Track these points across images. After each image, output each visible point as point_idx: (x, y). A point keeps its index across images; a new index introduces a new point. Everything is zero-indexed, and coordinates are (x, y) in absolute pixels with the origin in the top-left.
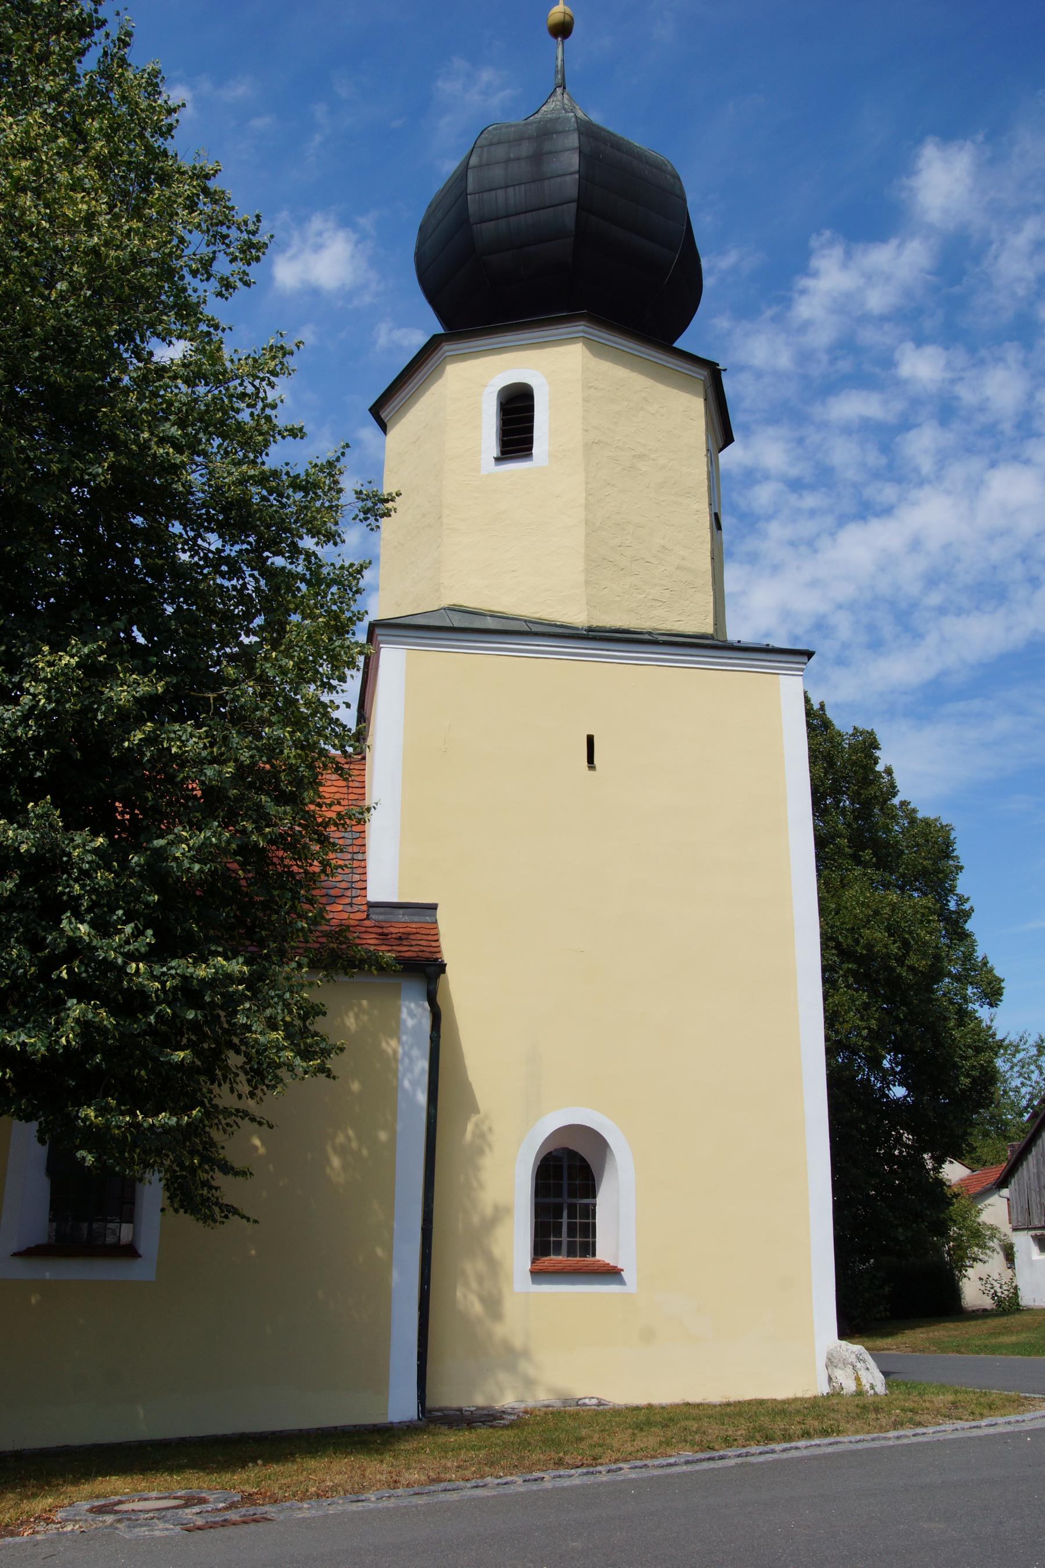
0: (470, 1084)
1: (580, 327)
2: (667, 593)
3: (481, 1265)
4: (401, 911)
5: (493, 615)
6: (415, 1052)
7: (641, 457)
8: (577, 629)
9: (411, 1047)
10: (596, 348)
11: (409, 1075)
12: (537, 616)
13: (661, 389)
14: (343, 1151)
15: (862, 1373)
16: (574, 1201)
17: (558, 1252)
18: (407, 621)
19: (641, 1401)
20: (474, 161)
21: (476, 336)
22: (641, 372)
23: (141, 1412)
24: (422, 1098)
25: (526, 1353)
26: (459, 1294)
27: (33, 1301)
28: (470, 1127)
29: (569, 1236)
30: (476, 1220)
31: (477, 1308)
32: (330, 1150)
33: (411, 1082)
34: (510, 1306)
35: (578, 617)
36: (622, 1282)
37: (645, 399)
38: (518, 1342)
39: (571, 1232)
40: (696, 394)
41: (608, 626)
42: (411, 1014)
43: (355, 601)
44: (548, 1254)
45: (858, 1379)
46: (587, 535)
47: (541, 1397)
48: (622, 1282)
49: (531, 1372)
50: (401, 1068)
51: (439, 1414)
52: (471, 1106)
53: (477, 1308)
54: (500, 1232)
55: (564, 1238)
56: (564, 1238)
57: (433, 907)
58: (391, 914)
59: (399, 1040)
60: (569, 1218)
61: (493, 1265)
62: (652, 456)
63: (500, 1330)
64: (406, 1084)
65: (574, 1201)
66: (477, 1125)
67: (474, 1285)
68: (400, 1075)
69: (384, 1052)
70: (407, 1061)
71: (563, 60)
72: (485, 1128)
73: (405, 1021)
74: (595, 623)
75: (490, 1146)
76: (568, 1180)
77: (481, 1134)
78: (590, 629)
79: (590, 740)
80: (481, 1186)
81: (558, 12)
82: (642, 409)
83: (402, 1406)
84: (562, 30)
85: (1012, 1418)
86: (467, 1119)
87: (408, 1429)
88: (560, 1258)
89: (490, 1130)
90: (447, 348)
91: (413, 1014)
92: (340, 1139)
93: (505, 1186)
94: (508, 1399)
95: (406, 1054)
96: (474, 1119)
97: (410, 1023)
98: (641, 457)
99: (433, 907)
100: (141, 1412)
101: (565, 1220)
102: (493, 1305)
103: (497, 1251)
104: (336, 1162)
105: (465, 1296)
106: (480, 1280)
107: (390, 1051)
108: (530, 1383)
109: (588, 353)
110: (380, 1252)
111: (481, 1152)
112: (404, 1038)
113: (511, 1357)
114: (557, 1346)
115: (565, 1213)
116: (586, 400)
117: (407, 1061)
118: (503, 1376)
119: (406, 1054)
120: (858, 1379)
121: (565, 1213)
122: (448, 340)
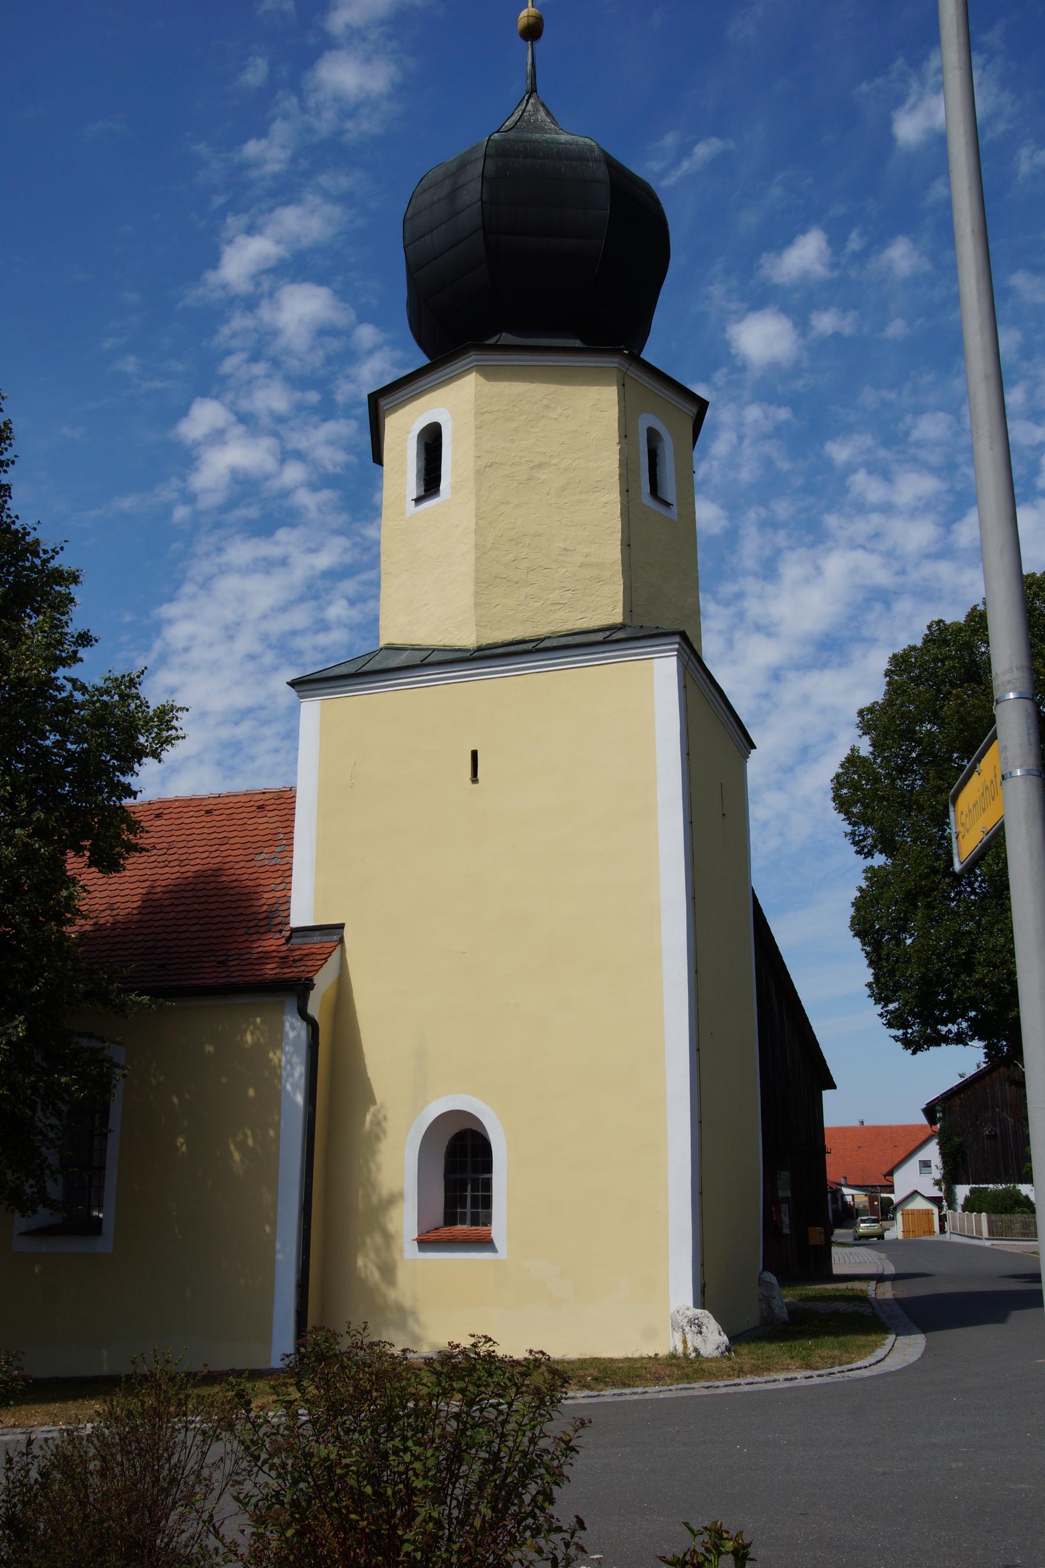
0: (369, 1079)
1: (472, 358)
2: (569, 594)
3: (378, 1238)
4: (317, 933)
5: (414, 648)
6: (295, 1059)
7: (540, 466)
8: (468, 650)
9: (292, 1056)
10: (490, 373)
11: (291, 1080)
12: (442, 643)
13: (567, 389)
14: (242, 1147)
15: (689, 1337)
16: (475, 1176)
17: (463, 1223)
18: (311, 677)
20: (408, 215)
21: (410, 382)
23: (105, 1354)
24: (300, 1099)
25: (413, 1313)
26: (360, 1262)
27: (37, 1271)
28: (369, 1117)
29: (472, 1207)
30: (374, 1199)
31: (376, 1275)
32: (232, 1148)
33: (292, 1085)
34: (402, 1275)
35: (468, 639)
37: (547, 407)
38: (408, 1303)
39: (474, 1205)
40: (613, 386)
41: (500, 641)
42: (293, 1028)
44: (455, 1224)
45: (685, 1342)
46: (477, 559)
49: (417, 1330)
50: (284, 1074)
52: (369, 1098)
53: (374, 1275)
55: (468, 1210)
56: (468, 1210)
57: (341, 926)
58: (306, 936)
59: (282, 1050)
60: (472, 1191)
61: (388, 1238)
62: (553, 462)
63: (392, 1295)
64: (289, 1087)
65: (475, 1176)
66: (374, 1115)
67: (372, 1255)
68: (283, 1081)
69: (271, 1060)
70: (288, 1067)
71: (533, 64)
72: (381, 1116)
73: (287, 1034)
74: (484, 642)
75: (384, 1132)
76: (463, 1161)
77: (377, 1123)
78: (480, 649)
79: (474, 754)
80: (379, 1168)
81: (526, 15)
82: (543, 417)
84: (533, 32)
85: (640, 1390)
86: (367, 1109)
88: (465, 1227)
89: (385, 1118)
91: (294, 1030)
92: (240, 1137)
93: (398, 1168)
95: (289, 1062)
96: (372, 1109)
97: (292, 1035)
98: (540, 466)
99: (341, 926)
100: (105, 1354)
101: (469, 1193)
102: (388, 1271)
103: (391, 1228)
104: (237, 1156)
105: (366, 1266)
106: (377, 1251)
107: (276, 1060)
109: (481, 380)
110: (268, 1229)
111: (378, 1139)
112: (287, 1048)
113: (402, 1315)
115: (469, 1187)
116: (478, 427)
117: (288, 1067)
119: (289, 1062)
120: (685, 1342)
121: (469, 1187)
122: (382, 396)
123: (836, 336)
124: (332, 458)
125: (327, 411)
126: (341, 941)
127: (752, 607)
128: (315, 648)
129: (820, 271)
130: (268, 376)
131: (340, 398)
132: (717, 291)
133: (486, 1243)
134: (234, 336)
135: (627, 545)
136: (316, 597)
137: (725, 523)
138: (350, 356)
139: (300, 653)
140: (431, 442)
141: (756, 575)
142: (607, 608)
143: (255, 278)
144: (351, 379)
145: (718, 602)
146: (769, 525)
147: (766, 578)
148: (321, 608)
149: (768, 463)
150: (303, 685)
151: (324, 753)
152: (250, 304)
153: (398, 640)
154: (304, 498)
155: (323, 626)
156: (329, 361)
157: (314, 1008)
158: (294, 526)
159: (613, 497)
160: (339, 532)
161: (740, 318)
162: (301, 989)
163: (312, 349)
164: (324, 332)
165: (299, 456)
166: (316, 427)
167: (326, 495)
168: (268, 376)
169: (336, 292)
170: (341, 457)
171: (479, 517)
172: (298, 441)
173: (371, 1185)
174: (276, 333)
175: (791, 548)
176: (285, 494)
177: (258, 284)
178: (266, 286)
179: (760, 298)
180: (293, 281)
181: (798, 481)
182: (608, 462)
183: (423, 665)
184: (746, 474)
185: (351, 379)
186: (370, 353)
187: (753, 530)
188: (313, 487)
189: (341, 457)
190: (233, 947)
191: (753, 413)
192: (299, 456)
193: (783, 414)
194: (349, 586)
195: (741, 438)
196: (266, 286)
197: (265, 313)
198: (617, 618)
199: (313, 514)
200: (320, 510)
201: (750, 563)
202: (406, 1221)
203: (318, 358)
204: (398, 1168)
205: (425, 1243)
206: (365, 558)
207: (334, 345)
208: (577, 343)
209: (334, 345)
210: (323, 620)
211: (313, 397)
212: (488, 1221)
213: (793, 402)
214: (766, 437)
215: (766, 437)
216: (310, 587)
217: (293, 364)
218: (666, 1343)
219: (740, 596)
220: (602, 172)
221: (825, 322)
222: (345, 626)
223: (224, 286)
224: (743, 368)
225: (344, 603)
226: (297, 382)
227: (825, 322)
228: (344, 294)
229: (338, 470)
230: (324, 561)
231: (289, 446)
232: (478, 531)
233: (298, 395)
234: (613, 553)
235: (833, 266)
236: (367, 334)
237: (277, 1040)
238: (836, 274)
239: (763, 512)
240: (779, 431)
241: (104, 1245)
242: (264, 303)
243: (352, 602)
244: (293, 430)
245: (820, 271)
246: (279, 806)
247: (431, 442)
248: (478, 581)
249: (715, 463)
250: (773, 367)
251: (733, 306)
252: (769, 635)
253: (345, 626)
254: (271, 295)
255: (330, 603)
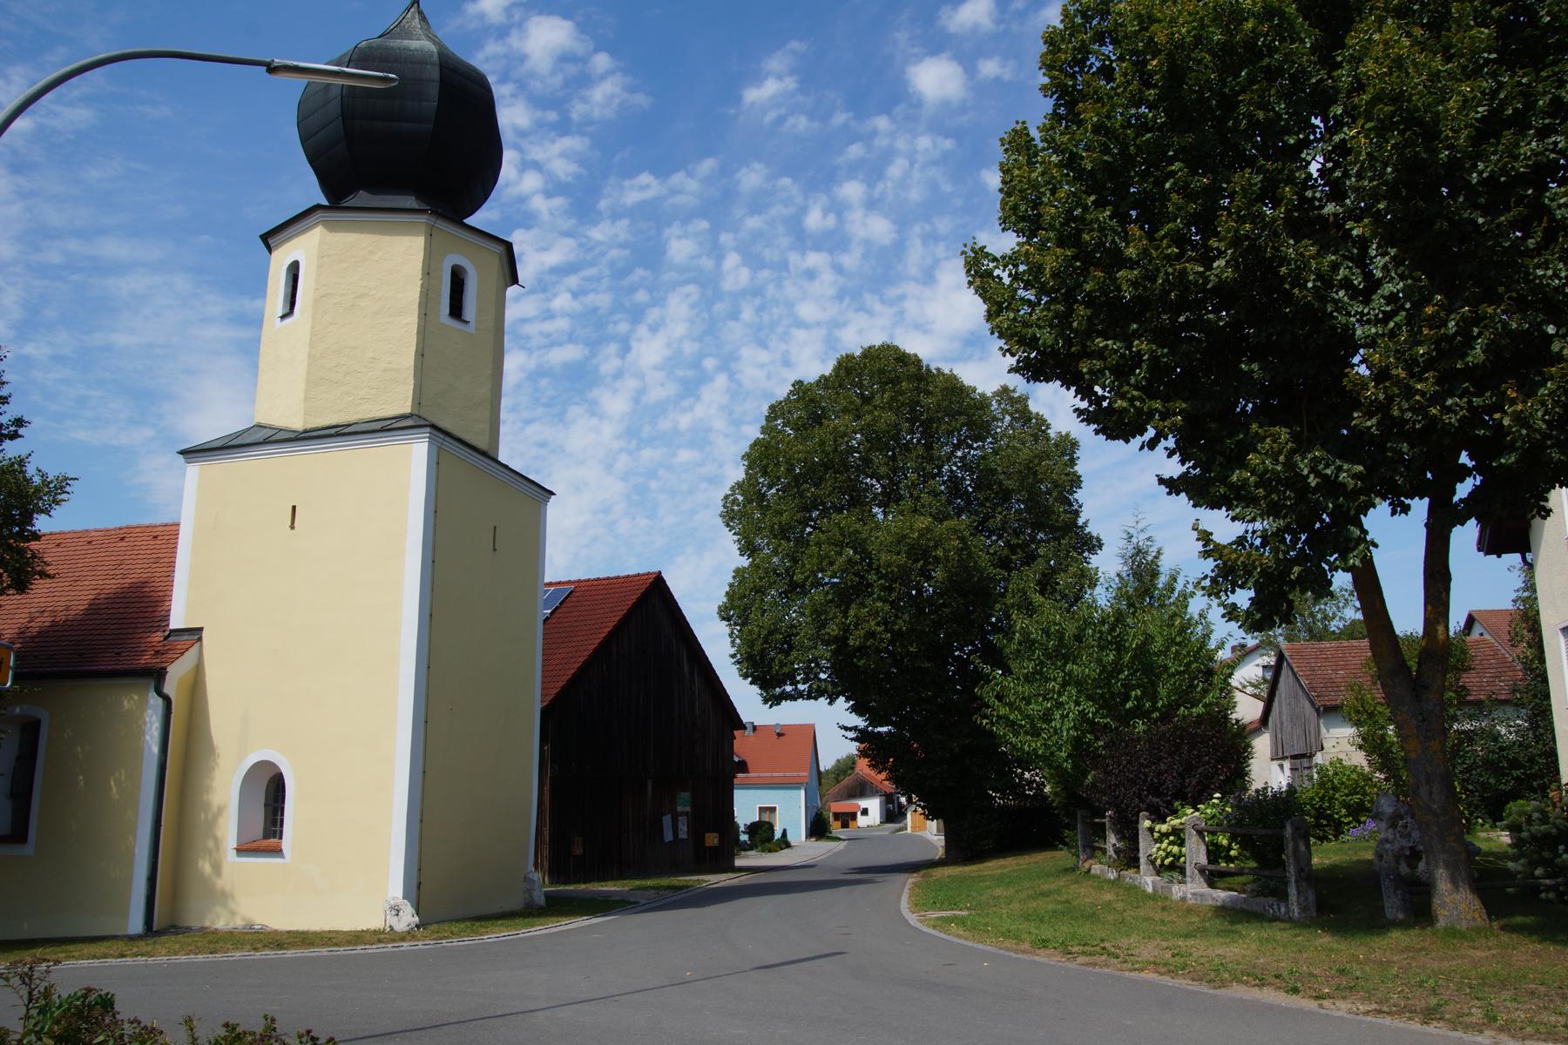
7: (362, 296)
13: (387, 238)
19: (327, 928)
22: (370, 232)
24: (156, 749)
25: (233, 897)
26: (201, 863)
34: (226, 870)
35: (298, 424)
36: (282, 856)
38: (228, 888)
40: (417, 235)
43: (1145, 21)
47: (239, 923)
48: (282, 856)
51: (1519, 919)
54: (221, 821)
57: (201, 629)
63: (220, 883)
74: (309, 426)
76: (271, 791)
78: (306, 431)
83: (136, 925)
87: (132, 938)
90: (319, 215)
91: (156, 702)
94: (222, 923)
98: (362, 296)
99: (201, 629)
102: (217, 868)
103: (219, 834)
108: (233, 913)
113: (224, 897)
114: (255, 894)
118: (219, 909)
123: (998, 79)
124: (563, 169)
125: (564, 127)
126: (200, 639)
127: (911, 307)
128: (541, 334)
129: (987, 23)
130: (513, 96)
131: (575, 116)
132: (902, 36)
133: (277, 852)
134: (487, 60)
135: (421, 354)
136: (544, 290)
137: (895, 235)
138: (584, 81)
139: (528, 338)
140: (294, 271)
141: (916, 280)
142: (400, 402)
143: (508, 11)
144: (585, 100)
145: (883, 302)
146: (930, 238)
147: (925, 283)
148: (548, 300)
149: (934, 186)
150: (190, 453)
151: (194, 500)
152: (502, 32)
153: (263, 422)
154: (539, 204)
155: (549, 315)
156: (567, 84)
157: (170, 688)
158: (528, 227)
159: (411, 321)
160: (567, 234)
161: (919, 59)
162: (157, 676)
163: (553, 73)
164: (565, 58)
165: (537, 166)
166: (553, 142)
167: (559, 201)
168: (513, 96)
169: (578, 24)
170: (573, 168)
171: (313, 334)
172: (537, 153)
173: (207, 806)
174: (523, 58)
175: (947, 258)
176: (522, 199)
177: (509, 16)
178: (517, 17)
179: (937, 44)
180: (540, 13)
181: (959, 202)
182: (411, 293)
183: (266, 442)
184: (915, 195)
185: (585, 100)
186: (603, 78)
187: (918, 242)
188: (548, 194)
189: (573, 168)
190: (123, 638)
191: (924, 142)
192: (537, 166)
193: (948, 144)
194: (573, 281)
195: (912, 164)
196: (517, 17)
197: (514, 40)
198: (407, 410)
199: (546, 217)
200: (551, 213)
201: (913, 271)
202: (228, 831)
203: (558, 80)
204: (225, 793)
205: (241, 851)
206: (588, 257)
207: (572, 69)
208: (411, 202)
209: (572, 69)
210: (548, 310)
211: (552, 116)
212: (280, 835)
213: (958, 135)
214: (935, 163)
215: (935, 163)
216: (540, 281)
217: (536, 86)
218: (372, 920)
219: (902, 298)
220: (435, 73)
221: (989, 68)
222: (568, 315)
223: (482, 16)
224: (919, 104)
225: (568, 296)
226: (538, 102)
227: (989, 68)
228: (583, 28)
229: (570, 179)
230: (553, 258)
231: (529, 157)
232: (312, 345)
233: (539, 114)
234: (408, 361)
235: (998, 22)
236: (602, 61)
237: (143, 704)
238: (1001, 27)
239: (927, 227)
240: (943, 160)
241: (28, 850)
242: (514, 32)
243: (575, 295)
244: (531, 143)
245: (987, 23)
246: (164, 538)
247: (294, 271)
248: (308, 382)
249: (889, 184)
250: (945, 104)
251: (915, 50)
252: (926, 332)
253: (568, 315)
254: (520, 25)
255: (555, 295)
